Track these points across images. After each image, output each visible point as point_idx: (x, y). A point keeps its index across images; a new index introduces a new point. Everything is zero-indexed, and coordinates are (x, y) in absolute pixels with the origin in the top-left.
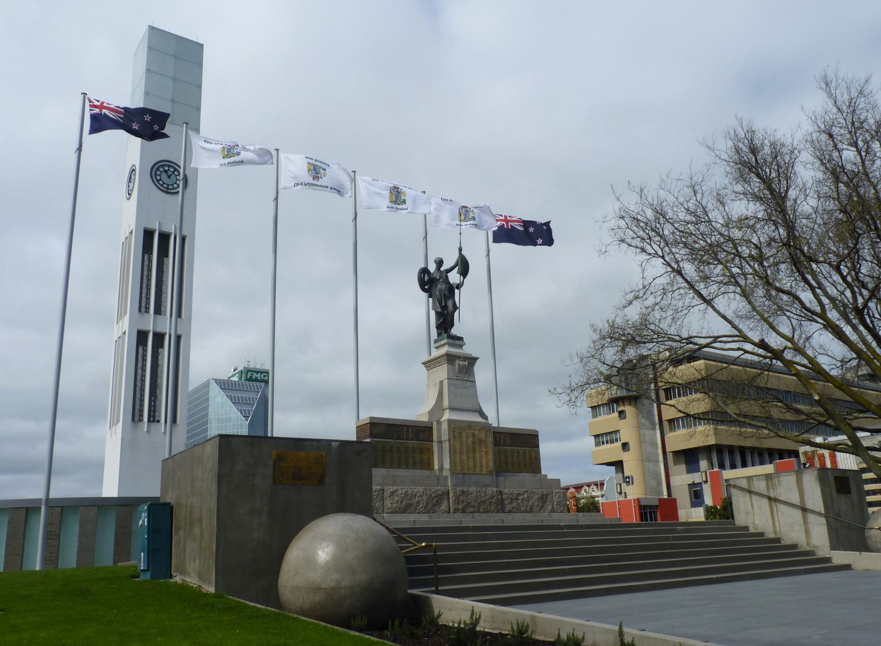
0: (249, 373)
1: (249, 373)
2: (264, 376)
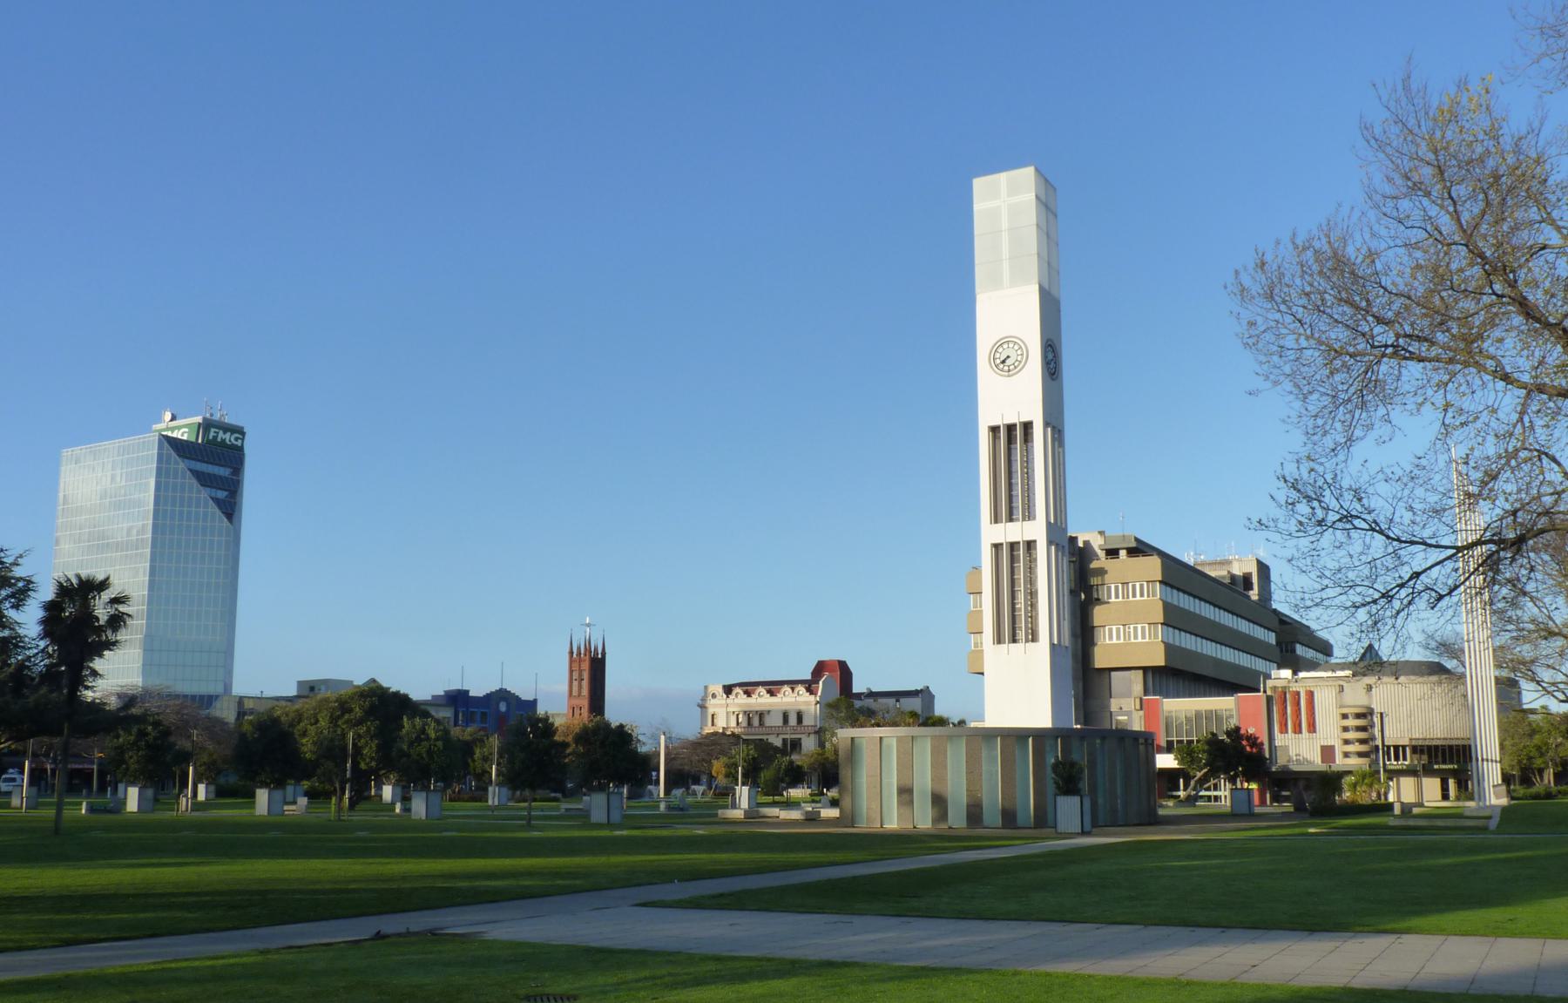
0: (213, 430)
1: (213, 430)
2: (236, 439)
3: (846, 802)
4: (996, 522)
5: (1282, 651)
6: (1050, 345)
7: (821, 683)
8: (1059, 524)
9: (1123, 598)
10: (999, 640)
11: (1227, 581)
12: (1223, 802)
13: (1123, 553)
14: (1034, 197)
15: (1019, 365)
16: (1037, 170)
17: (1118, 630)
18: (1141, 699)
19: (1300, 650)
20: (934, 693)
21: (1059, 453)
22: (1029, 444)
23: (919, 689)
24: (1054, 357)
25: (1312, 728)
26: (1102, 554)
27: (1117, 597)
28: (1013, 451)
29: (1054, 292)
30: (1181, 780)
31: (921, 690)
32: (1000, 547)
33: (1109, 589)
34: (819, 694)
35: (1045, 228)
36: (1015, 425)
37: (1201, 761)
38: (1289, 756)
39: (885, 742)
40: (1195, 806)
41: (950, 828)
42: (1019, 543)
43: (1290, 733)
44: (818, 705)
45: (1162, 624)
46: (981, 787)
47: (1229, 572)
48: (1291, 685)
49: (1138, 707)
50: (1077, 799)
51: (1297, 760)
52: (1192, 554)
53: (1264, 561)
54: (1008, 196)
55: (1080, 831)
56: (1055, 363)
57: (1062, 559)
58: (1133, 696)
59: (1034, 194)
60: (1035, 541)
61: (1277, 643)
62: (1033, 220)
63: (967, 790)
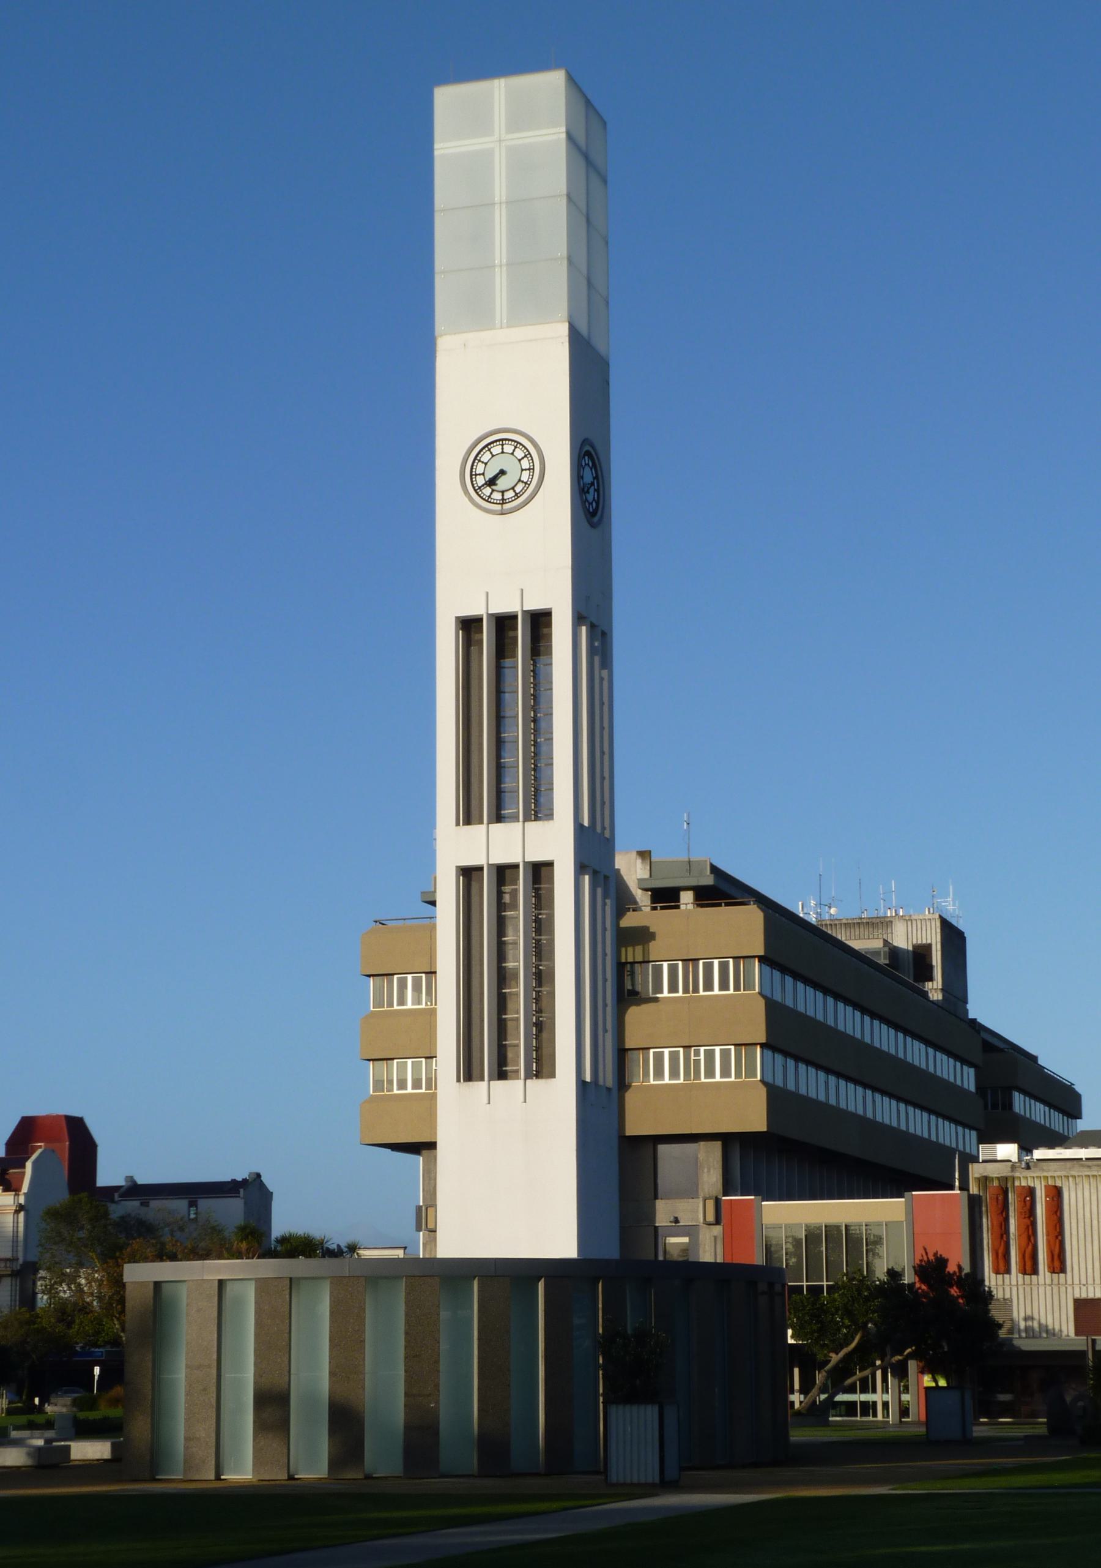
3: (139, 1428)
4: (468, 821)
5: (986, 1107)
6: (588, 453)
7: (29, 1165)
8: (599, 829)
9: (686, 990)
10: (469, 1072)
11: (883, 961)
12: (880, 1417)
13: (687, 897)
14: (564, 136)
15: (523, 492)
16: (571, 79)
17: (674, 1057)
18: (717, 1202)
19: (1020, 1103)
20: (271, 1189)
21: (602, 679)
22: (543, 659)
23: (239, 1179)
24: (596, 478)
25: (1058, 1264)
26: (643, 899)
27: (673, 988)
28: (507, 672)
29: (599, 344)
30: (796, 1371)
31: (245, 1181)
32: (474, 874)
33: (658, 971)
34: (25, 1188)
35: (583, 205)
36: (513, 617)
37: (839, 1330)
38: (1012, 1320)
39: (229, 1288)
40: (827, 1424)
41: (368, 1477)
42: (515, 867)
43: (1030, 1267)
44: (22, 1215)
45: (762, 1046)
46: (437, 1386)
47: (886, 942)
48: (1017, 1174)
49: (711, 1218)
50: (650, 1413)
51: (1027, 1329)
52: (813, 903)
53: (954, 922)
54: (508, 131)
55: (657, 1480)
56: (597, 490)
57: (604, 904)
58: (701, 1195)
59: (564, 129)
60: (550, 865)
61: (977, 1088)
62: (561, 186)
63: (407, 1394)
